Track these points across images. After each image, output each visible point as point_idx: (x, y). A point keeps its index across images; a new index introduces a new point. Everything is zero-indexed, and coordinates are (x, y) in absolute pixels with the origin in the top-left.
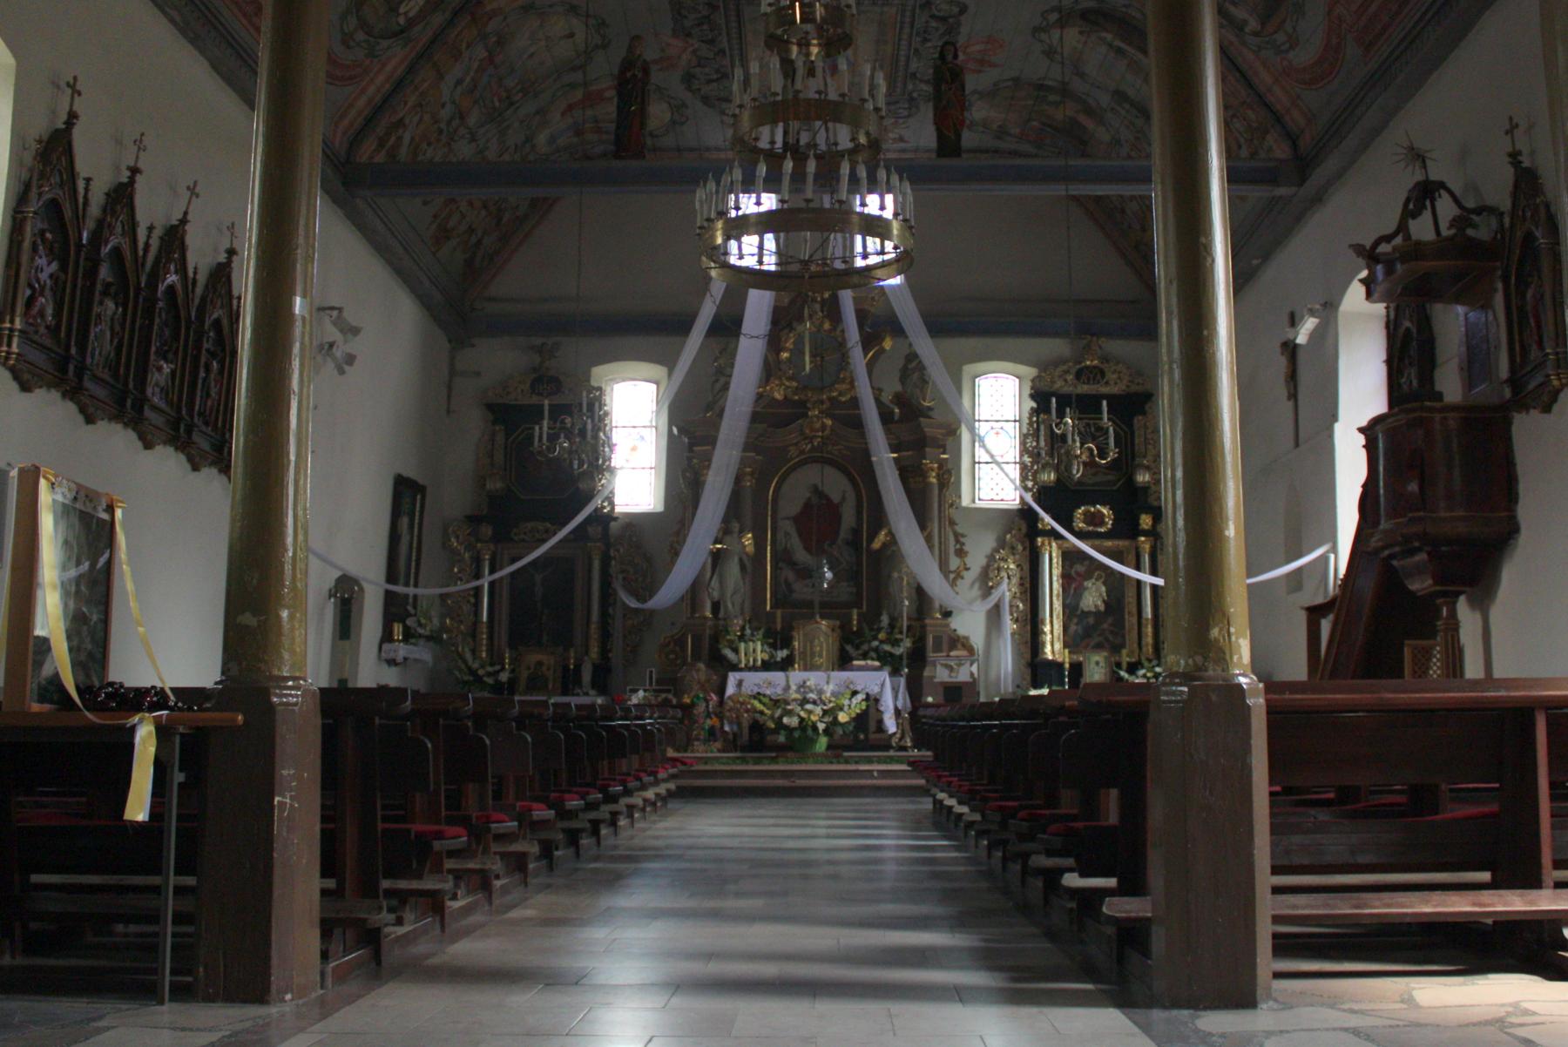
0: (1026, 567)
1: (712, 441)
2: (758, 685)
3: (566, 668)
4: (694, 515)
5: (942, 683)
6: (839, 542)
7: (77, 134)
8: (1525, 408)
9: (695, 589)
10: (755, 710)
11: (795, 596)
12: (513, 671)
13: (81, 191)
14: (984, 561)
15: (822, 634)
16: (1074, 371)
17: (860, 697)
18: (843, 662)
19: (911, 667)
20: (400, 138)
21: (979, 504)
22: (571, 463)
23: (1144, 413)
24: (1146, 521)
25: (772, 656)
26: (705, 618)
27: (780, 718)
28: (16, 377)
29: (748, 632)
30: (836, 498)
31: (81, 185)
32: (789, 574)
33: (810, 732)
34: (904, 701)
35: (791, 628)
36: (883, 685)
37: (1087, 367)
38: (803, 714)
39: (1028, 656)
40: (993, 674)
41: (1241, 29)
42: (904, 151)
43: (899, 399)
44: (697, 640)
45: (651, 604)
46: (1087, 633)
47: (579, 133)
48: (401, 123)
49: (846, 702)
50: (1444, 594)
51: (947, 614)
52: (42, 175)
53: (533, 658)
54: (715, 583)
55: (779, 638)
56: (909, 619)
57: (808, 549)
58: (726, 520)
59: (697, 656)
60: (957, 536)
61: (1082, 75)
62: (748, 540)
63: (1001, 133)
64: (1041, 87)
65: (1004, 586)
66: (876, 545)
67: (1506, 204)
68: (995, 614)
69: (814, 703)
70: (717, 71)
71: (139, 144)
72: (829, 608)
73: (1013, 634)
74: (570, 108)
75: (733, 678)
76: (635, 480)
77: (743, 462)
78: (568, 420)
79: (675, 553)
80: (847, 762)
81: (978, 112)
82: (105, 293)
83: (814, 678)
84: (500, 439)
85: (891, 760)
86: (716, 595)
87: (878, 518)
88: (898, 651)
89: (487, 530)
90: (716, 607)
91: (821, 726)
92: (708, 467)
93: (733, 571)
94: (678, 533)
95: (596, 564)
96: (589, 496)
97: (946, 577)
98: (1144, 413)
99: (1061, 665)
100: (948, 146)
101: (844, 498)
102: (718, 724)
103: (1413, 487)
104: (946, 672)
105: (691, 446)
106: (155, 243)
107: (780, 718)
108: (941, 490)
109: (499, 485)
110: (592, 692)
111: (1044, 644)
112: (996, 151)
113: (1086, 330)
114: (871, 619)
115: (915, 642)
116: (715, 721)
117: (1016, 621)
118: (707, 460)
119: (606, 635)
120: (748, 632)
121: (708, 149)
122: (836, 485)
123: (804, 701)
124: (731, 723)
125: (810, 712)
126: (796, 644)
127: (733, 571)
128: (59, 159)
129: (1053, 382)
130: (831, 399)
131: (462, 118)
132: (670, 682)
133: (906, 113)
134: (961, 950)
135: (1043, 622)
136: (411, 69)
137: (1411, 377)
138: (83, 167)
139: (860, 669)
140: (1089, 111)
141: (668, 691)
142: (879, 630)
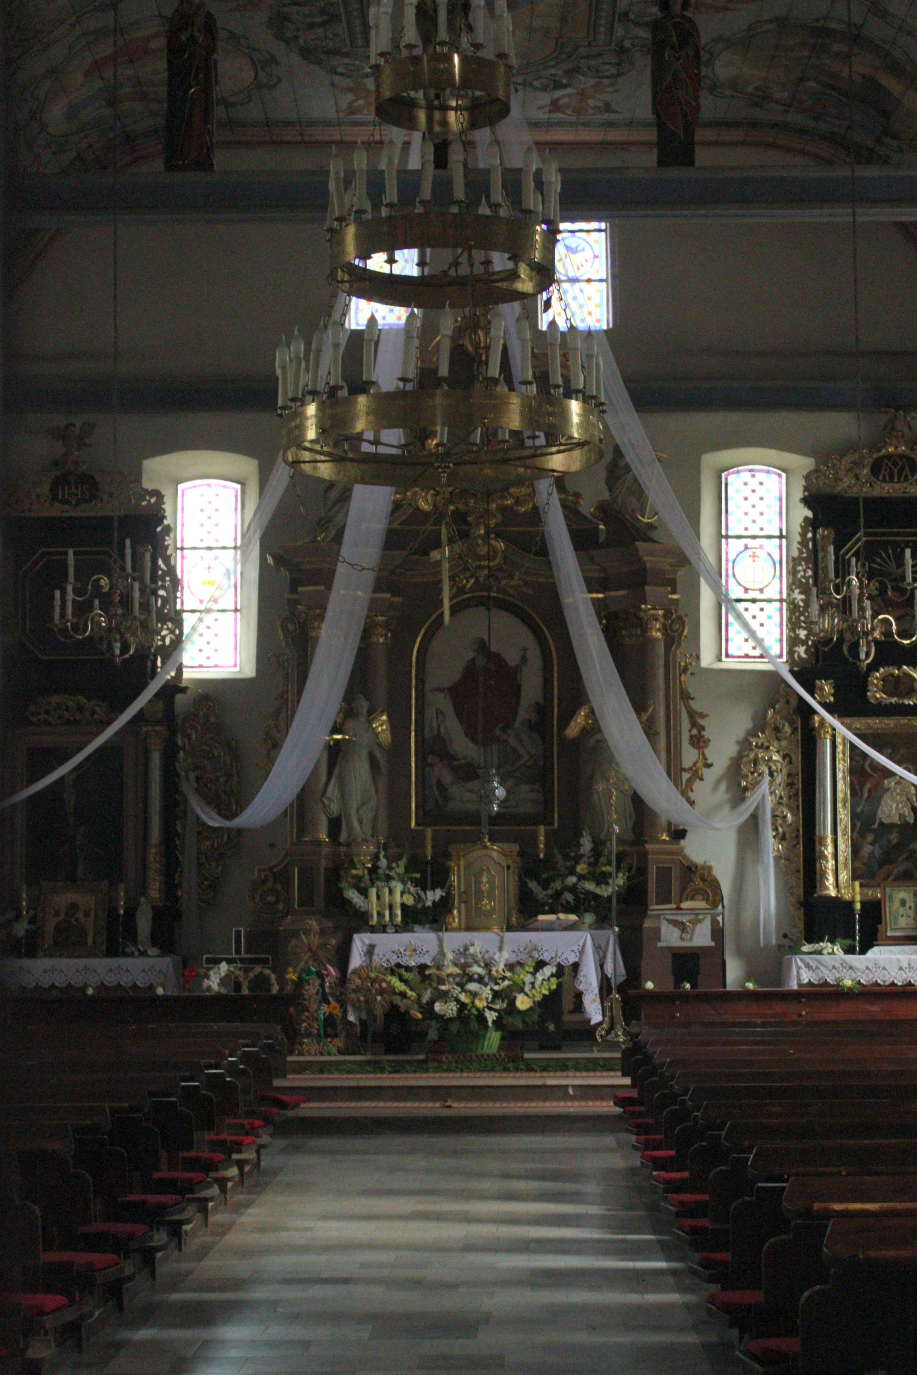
0: (797, 758)
1: (326, 578)
2: (398, 953)
3: (112, 911)
4: (298, 701)
5: (669, 948)
6: (517, 724)
9: (302, 806)
10: (393, 991)
11: (452, 805)
12: (33, 920)
14: (733, 750)
15: (489, 867)
16: (869, 461)
17: (548, 971)
18: (525, 911)
19: (626, 916)
21: (728, 664)
22: (110, 648)
25: (418, 899)
26: (319, 843)
27: (431, 1003)
29: (383, 863)
30: (512, 657)
33: (474, 1025)
34: (615, 967)
35: (448, 856)
36: (582, 952)
37: (889, 457)
38: (463, 997)
39: (800, 891)
40: (747, 917)
42: (610, 125)
43: (605, 510)
44: (307, 875)
45: (237, 822)
46: (888, 858)
47: (112, 102)
49: (528, 979)
51: (679, 834)
53: (63, 899)
54: (333, 790)
55: (430, 873)
56: (621, 841)
57: (471, 735)
58: (349, 697)
59: (306, 900)
60: (692, 714)
61: (884, 15)
62: (382, 724)
63: (761, 97)
64: (823, 32)
65: (765, 787)
66: (573, 730)
68: (750, 831)
69: (480, 980)
70: (322, 12)
72: (505, 826)
73: (777, 859)
74: (97, 66)
75: (360, 942)
76: (215, 634)
77: (374, 607)
78: (104, 582)
79: (274, 745)
80: (530, 1068)
81: (725, 68)
83: (481, 943)
85: (593, 1065)
86: (334, 807)
87: (575, 694)
88: (605, 891)
90: (335, 825)
91: (491, 1016)
92: (322, 617)
93: (359, 771)
94: (276, 714)
95: (156, 759)
96: (141, 667)
97: (677, 782)
99: (850, 904)
100: (675, 147)
101: (524, 659)
102: (338, 1012)
104: (676, 932)
105: (294, 585)
107: (431, 1003)
108: (668, 648)
110: (152, 951)
111: (823, 874)
112: (753, 124)
113: (887, 400)
114: (565, 841)
115: (636, 879)
116: (334, 1007)
117: (783, 838)
118: (319, 608)
119: (171, 866)
120: (383, 863)
121: (312, 124)
122: (511, 639)
123: (466, 978)
124: (357, 1009)
125: (474, 995)
126: (454, 879)
127: (359, 771)
129: (838, 479)
130: (504, 510)
132: (267, 944)
133: (614, 71)
134: (769, 910)
135: (822, 842)
139: (549, 928)
140: (895, 68)
141: (264, 962)
142: (578, 859)
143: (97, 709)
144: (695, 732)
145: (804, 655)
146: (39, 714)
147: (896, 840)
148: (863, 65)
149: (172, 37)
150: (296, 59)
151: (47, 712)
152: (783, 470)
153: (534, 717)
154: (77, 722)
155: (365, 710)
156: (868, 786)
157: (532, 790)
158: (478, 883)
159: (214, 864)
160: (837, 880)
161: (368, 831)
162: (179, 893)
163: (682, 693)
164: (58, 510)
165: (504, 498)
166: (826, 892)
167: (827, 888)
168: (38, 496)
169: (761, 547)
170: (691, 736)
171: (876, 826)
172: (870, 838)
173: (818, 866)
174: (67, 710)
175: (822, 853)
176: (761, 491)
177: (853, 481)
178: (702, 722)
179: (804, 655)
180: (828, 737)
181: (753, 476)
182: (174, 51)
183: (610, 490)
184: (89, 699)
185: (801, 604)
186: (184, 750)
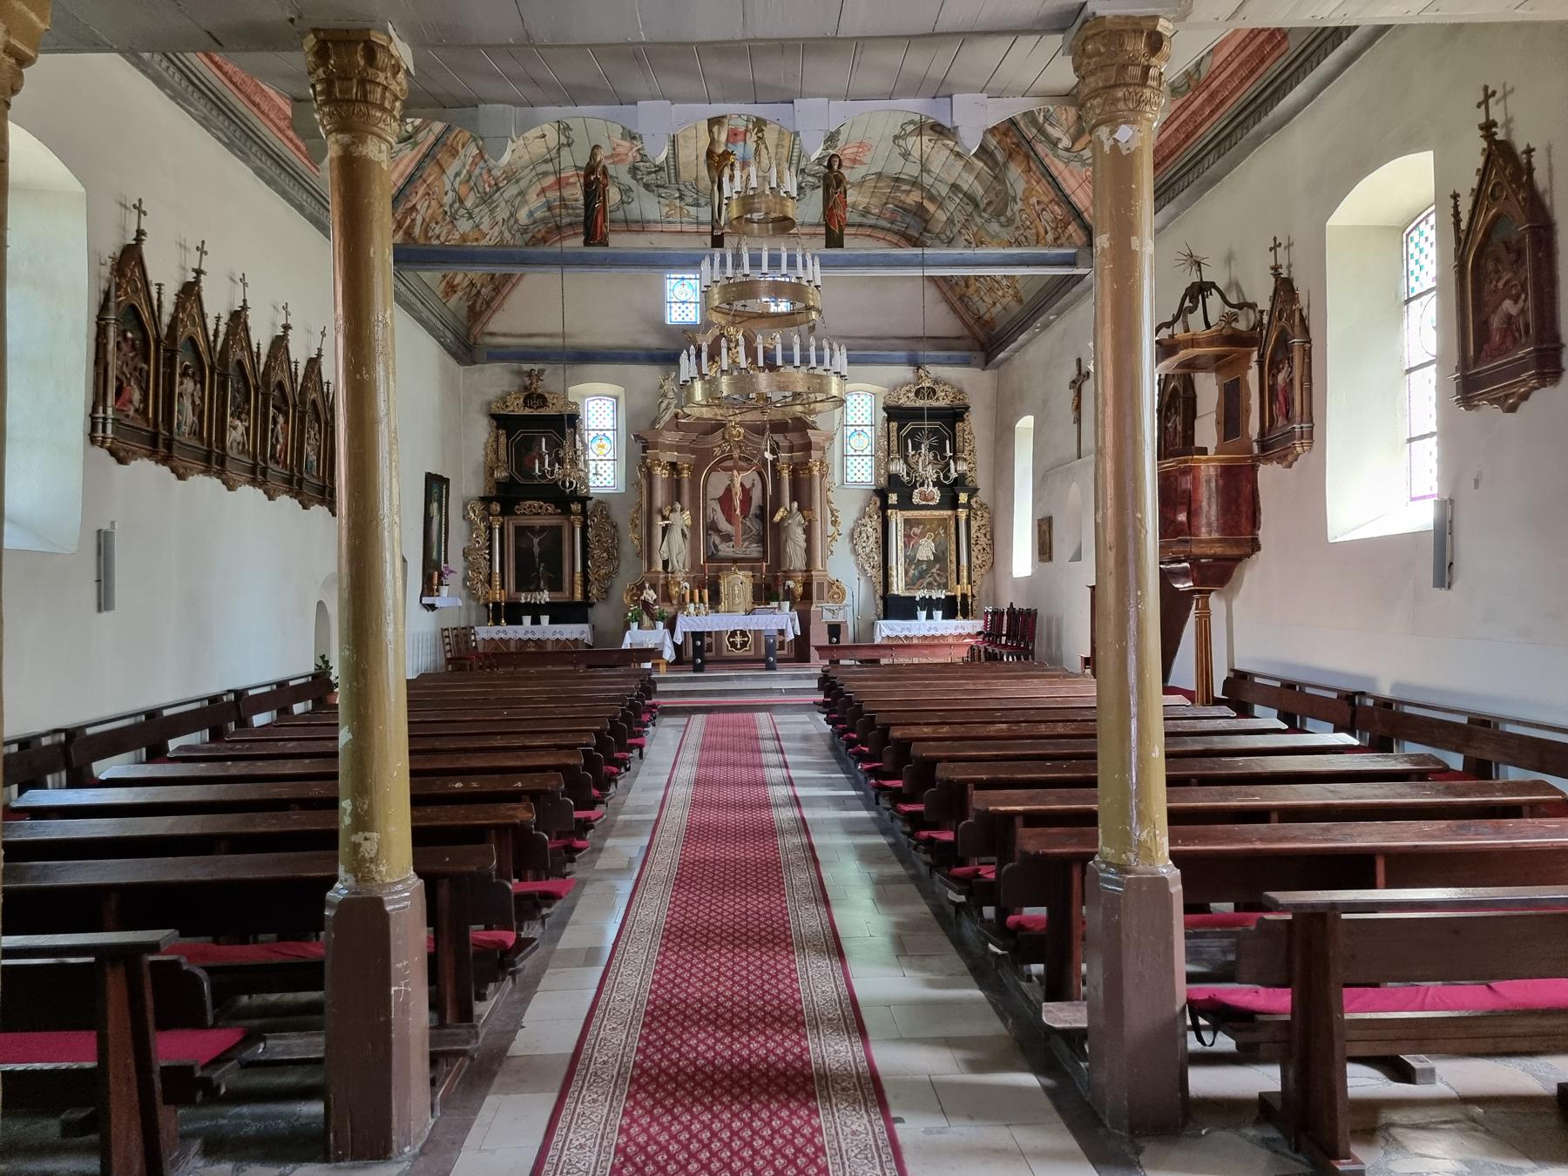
7: (147, 249)
8: (1268, 459)
13: (155, 295)
20: (413, 220)
23: (963, 420)
24: (963, 498)
28: (113, 453)
31: (154, 291)
32: (716, 539)
41: (1056, 145)
46: (922, 576)
47: (550, 209)
48: (413, 208)
50: (1199, 592)
52: (119, 287)
61: (928, 172)
63: (866, 212)
66: (777, 518)
67: (1264, 304)
71: (201, 250)
74: (543, 190)
82: (184, 374)
84: (503, 440)
89: (496, 507)
90: (666, 563)
95: (578, 531)
98: (963, 420)
103: (1182, 517)
105: (645, 449)
106: (223, 329)
109: (504, 474)
128: (133, 272)
131: (461, 202)
136: (420, 166)
137: (1177, 421)
138: (153, 277)
140: (932, 198)
148: (914, 198)
149: (586, 177)
150: (642, 190)
160: (898, 587)
164: (527, 412)
182: (588, 185)
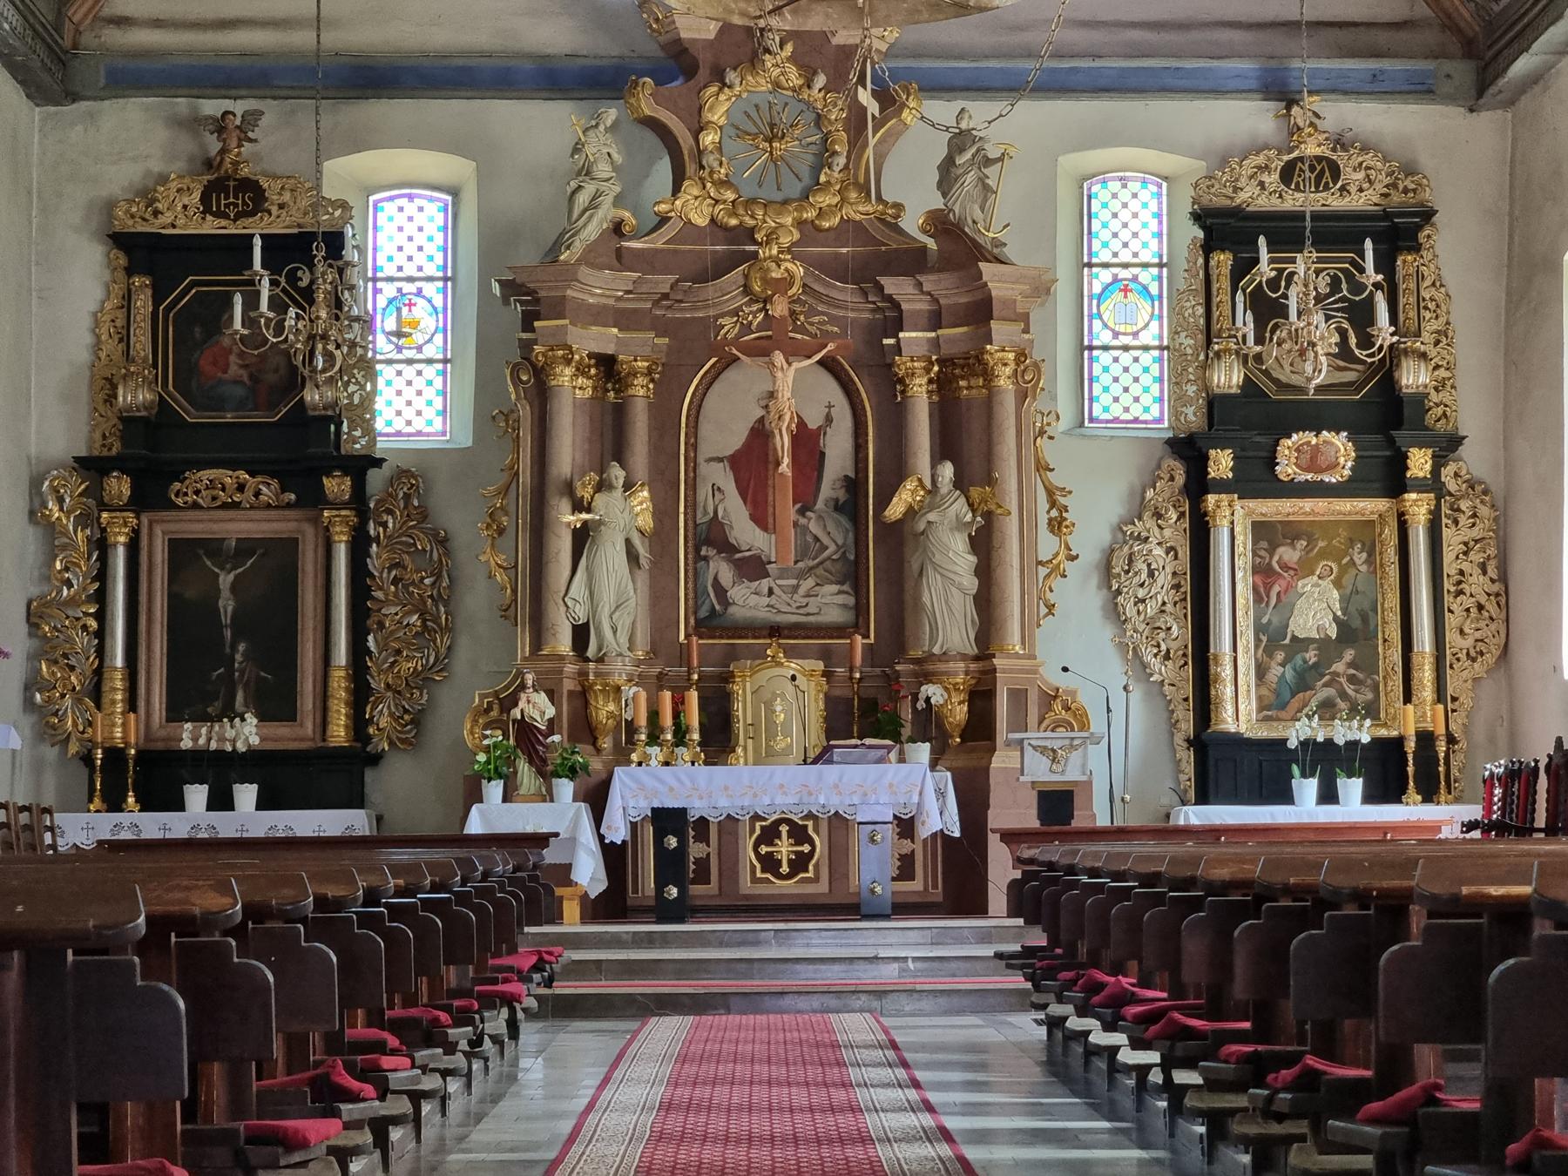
0: (1185, 552)
6: (820, 505)
60: (1050, 493)
66: (896, 510)
86: (581, 615)
90: (581, 634)
101: (829, 419)
104: (1045, 762)
143: (264, 489)
144: (1054, 513)
145: (1191, 418)
146: (186, 494)
147: (1314, 660)
151: (197, 492)
152: (1166, 179)
153: (842, 495)
154: (235, 506)
155: (621, 481)
156: (1276, 589)
157: (840, 592)
158: (770, 711)
159: (417, 693)
160: (1238, 714)
161: (623, 639)
162: (371, 731)
163: (1038, 461)
164: (211, 226)
165: (800, 209)
166: (1222, 727)
167: (1224, 721)
168: (185, 207)
169: (1135, 279)
170: (1050, 520)
171: (1287, 641)
172: (1280, 656)
173: (1213, 692)
174: (223, 490)
175: (1217, 675)
176: (1134, 205)
177: (1257, 190)
178: (1062, 500)
179: (1191, 418)
180: (1226, 522)
181: (1124, 186)
183: (944, 195)
184: (252, 475)
185: (1189, 351)
186: (378, 544)
